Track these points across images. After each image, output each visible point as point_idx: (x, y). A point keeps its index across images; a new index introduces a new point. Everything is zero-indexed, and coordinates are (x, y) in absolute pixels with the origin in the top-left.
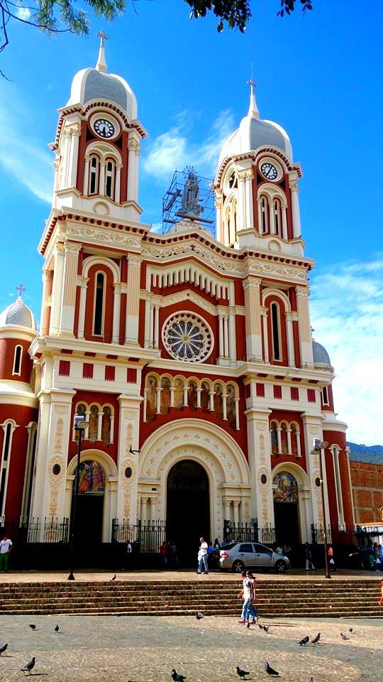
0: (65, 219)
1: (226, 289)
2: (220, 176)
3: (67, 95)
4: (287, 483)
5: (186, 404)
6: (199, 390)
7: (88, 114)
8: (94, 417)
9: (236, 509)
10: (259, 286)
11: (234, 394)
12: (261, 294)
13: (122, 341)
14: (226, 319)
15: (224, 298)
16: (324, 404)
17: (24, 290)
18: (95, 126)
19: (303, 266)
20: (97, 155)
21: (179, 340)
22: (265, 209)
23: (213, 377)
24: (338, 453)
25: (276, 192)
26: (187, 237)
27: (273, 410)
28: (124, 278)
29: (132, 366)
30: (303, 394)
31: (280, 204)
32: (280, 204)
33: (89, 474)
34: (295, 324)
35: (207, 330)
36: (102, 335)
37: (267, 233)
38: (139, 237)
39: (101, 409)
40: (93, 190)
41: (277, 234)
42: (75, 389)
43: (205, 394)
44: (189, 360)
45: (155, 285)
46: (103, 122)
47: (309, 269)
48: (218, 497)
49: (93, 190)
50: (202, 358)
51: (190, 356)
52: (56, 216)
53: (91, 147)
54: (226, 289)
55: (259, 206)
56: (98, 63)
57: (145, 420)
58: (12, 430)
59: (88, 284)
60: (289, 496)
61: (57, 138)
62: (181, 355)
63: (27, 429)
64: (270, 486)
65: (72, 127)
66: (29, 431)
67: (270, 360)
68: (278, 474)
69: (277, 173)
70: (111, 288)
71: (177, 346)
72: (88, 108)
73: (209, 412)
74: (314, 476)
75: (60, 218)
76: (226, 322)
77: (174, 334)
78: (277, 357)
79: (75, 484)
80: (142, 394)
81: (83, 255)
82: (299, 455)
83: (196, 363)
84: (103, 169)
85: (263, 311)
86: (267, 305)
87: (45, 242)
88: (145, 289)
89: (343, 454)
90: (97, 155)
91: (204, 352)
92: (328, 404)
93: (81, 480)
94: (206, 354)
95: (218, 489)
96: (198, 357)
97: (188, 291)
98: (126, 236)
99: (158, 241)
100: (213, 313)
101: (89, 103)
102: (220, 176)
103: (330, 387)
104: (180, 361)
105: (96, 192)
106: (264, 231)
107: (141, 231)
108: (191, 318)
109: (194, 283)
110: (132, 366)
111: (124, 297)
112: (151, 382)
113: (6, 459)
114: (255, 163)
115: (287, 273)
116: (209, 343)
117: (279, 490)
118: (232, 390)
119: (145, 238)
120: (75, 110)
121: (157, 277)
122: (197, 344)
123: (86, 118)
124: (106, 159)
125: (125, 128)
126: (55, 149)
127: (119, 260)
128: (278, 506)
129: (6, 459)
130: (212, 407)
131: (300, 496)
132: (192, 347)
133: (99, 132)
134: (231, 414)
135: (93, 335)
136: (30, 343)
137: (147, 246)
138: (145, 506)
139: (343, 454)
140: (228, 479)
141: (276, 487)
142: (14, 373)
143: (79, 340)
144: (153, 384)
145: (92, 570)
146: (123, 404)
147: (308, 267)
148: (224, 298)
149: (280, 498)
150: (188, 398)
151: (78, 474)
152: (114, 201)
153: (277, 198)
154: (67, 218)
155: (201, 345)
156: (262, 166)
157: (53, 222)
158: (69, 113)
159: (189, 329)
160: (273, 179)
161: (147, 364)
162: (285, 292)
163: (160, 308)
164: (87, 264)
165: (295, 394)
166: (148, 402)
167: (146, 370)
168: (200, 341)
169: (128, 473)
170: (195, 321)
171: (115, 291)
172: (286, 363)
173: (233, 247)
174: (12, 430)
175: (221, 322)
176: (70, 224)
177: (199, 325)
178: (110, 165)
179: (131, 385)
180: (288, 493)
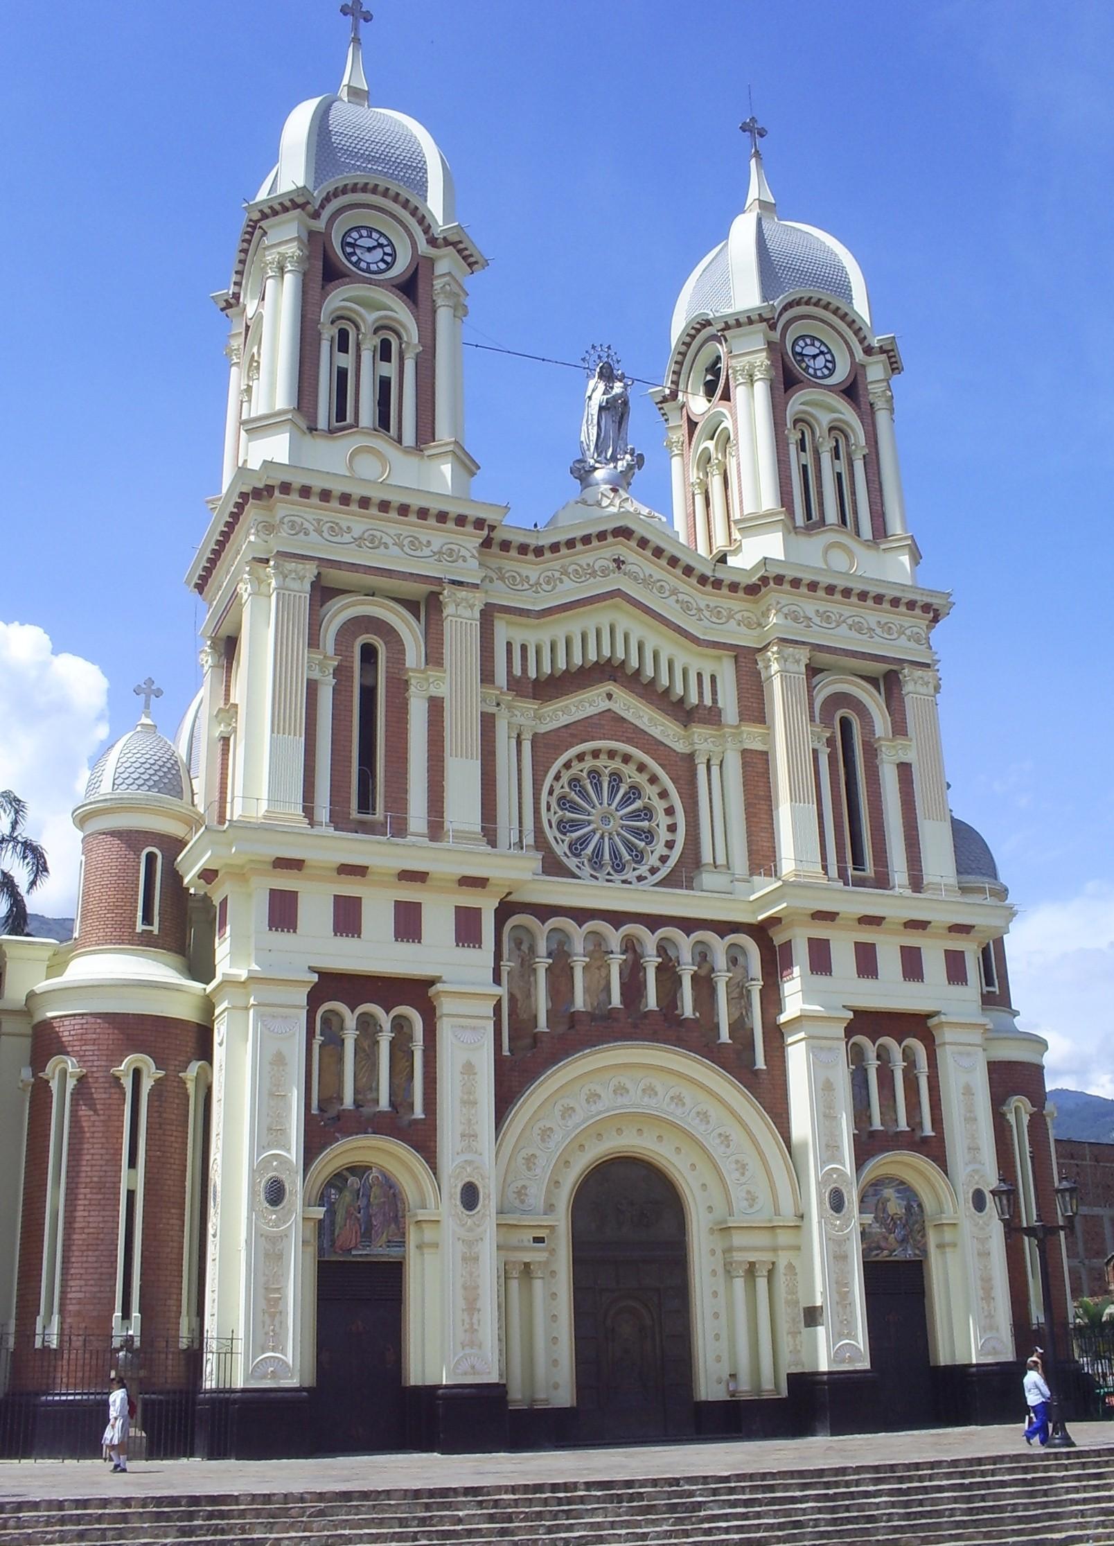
0: (271, 495)
1: (713, 678)
2: (676, 367)
3: (271, 157)
4: (895, 1207)
5: (616, 1000)
6: (652, 962)
7: (326, 214)
8: (366, 1045)
9: (762, 1283)
10: (803, 669)
11: (746, 969)
12: (810, 689)
13: (436, 829)
14: (715, 762)
15: (708, 701)
16: (986, 989)
17: (158, 693)
18: (344, 244)
19: (918, 611)
20: (349, 319)
21: (589, 823)
22: (808, 458)
23: (688, 925)
24: (1026, 1119)
25: (834, 410)
26: (602, 536)
27: (855, 1012)
28: (434, 657)
29: (469, 899)
30: (934, 965)
31: (848, 445)
32: (848, 445)
33: (362, 1202)
34: (904, 769)
35: (663, 795)
36: (379, 814)
37: (814, 523)
38: (470, 541)
39: (350, 1020)
40: (341, 416)
41: (844, 522)
42: (312, 969)
43: (668, 972)
44: (616, 877)
45: (517, 671)
46: (364, 233)
47: (935, 620)
48: (713, 1252)
49: (341, 416)
50: (653, 871)
51: (619, 867)
52: (246, 489)
53: (338, 298)
54: (713, 678)
55: (793, 449)
56: (345, 81)
57: (506, 1053)
58: (147, 1085)
59: (337, 672)
60: (903, 1241)
61: (234, 278)
62: (596, 861)
63: (183, 1082)
64: (854, 1219)
65: (282, 249)
66: (191, 1086)
67: (842, 874)
68: (872, 1185)
69: (833, 362)
70: (399, 686)
71: (584, 841)
72: (327, 199)
73: (682, 1022)
74: (991, 1217)
75: (257, 493)
76: (715, 770)
77: (575, 808)
78: (858, 861)
79: (324, 1231)
80: (497, 980)
81: (323, 593)
82: (928, 1131)
83: (640, 886)
84: (366, 356)
85: (812, 737)
86: (826, 721)
87: (209, 560)
88: (493, 682)
89: (1037, 1124)
90: (349, 319)
91: (657, 855)
92: (996, 989)
93: (339, 1219)
94: (663, 859)
95: (712, 1231)
96: (643, 870)
97: (610, 687)
98: (437, 537)
99: (523, 549)
100: (680, 747)
101: (329, 185)
102: (680, 358)
103: (999, 943)
104: (594, 882)
105: (350, 418)
106: (809, 517)
107: (479, 523)
108: (618, 759)
109: (623, 662)
110: (469, 899)
111: (436, 707)
112: (518, 943)
113: (132, 1164)
114: (776, 336)
115: (878, 631)
116: (672, 828)
117: (876, 1229)
118: (741, 959)
119: (487, 543)
120: (293, 203)
121: (524, 648)
122: (637, 832)
123: (320, 225)
124: (376, 331)
125: (423, 247)
126: (229, 305)
127: (418, 603)
128: (875, 1272)
129: (132, 1164)
130: (688, 1008)
131: (932, 1239)
132: (589, 801)
133: (354, 259)
134: (740, 1027)
135: (355, 815)
136: (180, 844)
137: (494, 562)
138: (514, 1285)
139: (1037, 1124)
140: (739, 1203)
141: (869, 1218)
142: (140, 927)
143: (317, 830)
144: (525, 947)
145: (411, 1451)
146: (446, 1006)
147: (931, 615)
148: (708, 701)
149: (879, 1248)
150: (623, 985)
151: (331, 1205)
152: (400, 441)
153: (836, 429)
154: (277, 493)
155: (649, 836)
156: (795, 343)
157: (237, 505)
158: (275, 213)
159: (613, 791)
160: (825, 377)
161: (509, 894)
162: (873, 681)
163: (535, 735)
164: (335, 616)
165: (912, 965)
166: (512, 998)
167: (505, 910)
168: (638, 804)
169: (470, 1196)
170: (629, 770)
171: (412, 689)
172: (882, 881)
173: (722, 559)
174: (147, 1085)
175: (702, 770)
176: (284, 508)
177: (641, 779)
178: (386, 345)
179: (469, 954)
180: (899, 1233)
